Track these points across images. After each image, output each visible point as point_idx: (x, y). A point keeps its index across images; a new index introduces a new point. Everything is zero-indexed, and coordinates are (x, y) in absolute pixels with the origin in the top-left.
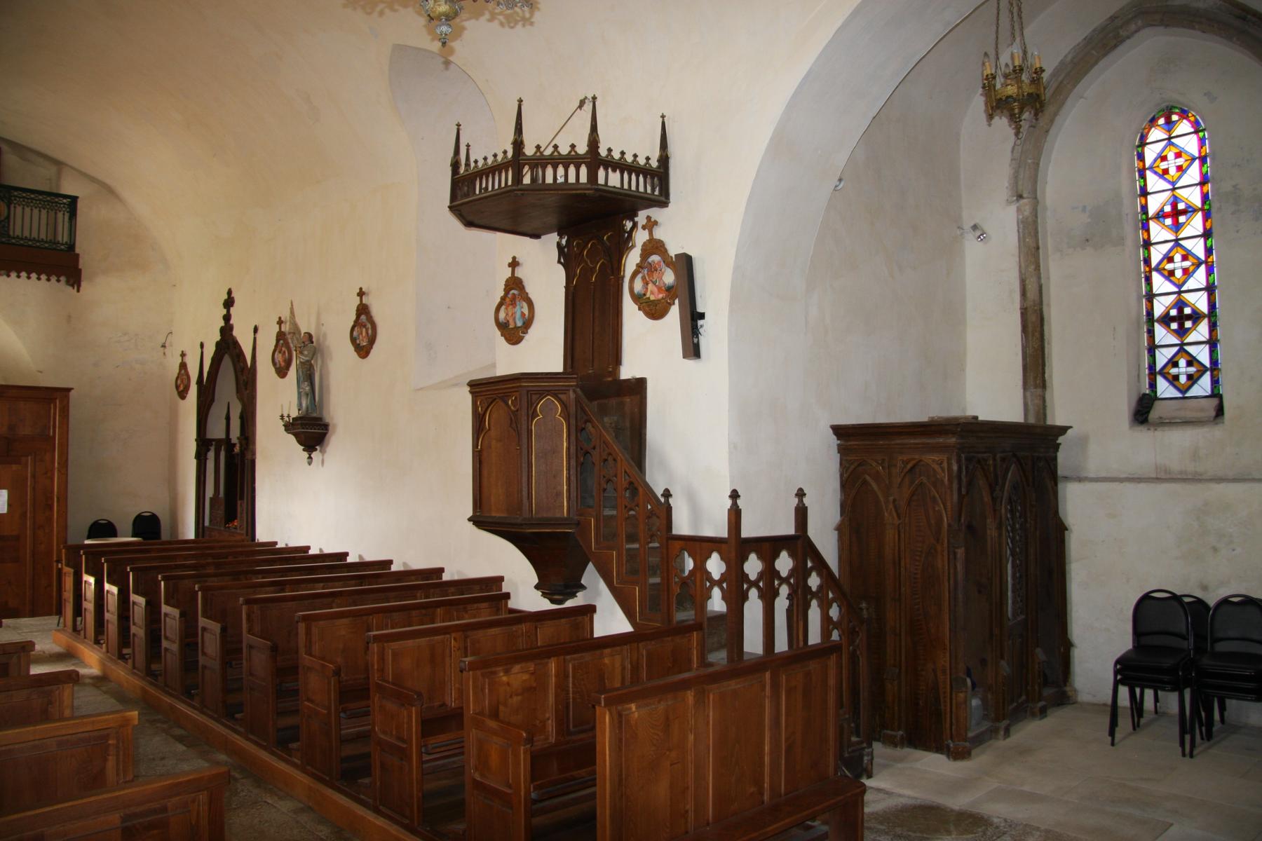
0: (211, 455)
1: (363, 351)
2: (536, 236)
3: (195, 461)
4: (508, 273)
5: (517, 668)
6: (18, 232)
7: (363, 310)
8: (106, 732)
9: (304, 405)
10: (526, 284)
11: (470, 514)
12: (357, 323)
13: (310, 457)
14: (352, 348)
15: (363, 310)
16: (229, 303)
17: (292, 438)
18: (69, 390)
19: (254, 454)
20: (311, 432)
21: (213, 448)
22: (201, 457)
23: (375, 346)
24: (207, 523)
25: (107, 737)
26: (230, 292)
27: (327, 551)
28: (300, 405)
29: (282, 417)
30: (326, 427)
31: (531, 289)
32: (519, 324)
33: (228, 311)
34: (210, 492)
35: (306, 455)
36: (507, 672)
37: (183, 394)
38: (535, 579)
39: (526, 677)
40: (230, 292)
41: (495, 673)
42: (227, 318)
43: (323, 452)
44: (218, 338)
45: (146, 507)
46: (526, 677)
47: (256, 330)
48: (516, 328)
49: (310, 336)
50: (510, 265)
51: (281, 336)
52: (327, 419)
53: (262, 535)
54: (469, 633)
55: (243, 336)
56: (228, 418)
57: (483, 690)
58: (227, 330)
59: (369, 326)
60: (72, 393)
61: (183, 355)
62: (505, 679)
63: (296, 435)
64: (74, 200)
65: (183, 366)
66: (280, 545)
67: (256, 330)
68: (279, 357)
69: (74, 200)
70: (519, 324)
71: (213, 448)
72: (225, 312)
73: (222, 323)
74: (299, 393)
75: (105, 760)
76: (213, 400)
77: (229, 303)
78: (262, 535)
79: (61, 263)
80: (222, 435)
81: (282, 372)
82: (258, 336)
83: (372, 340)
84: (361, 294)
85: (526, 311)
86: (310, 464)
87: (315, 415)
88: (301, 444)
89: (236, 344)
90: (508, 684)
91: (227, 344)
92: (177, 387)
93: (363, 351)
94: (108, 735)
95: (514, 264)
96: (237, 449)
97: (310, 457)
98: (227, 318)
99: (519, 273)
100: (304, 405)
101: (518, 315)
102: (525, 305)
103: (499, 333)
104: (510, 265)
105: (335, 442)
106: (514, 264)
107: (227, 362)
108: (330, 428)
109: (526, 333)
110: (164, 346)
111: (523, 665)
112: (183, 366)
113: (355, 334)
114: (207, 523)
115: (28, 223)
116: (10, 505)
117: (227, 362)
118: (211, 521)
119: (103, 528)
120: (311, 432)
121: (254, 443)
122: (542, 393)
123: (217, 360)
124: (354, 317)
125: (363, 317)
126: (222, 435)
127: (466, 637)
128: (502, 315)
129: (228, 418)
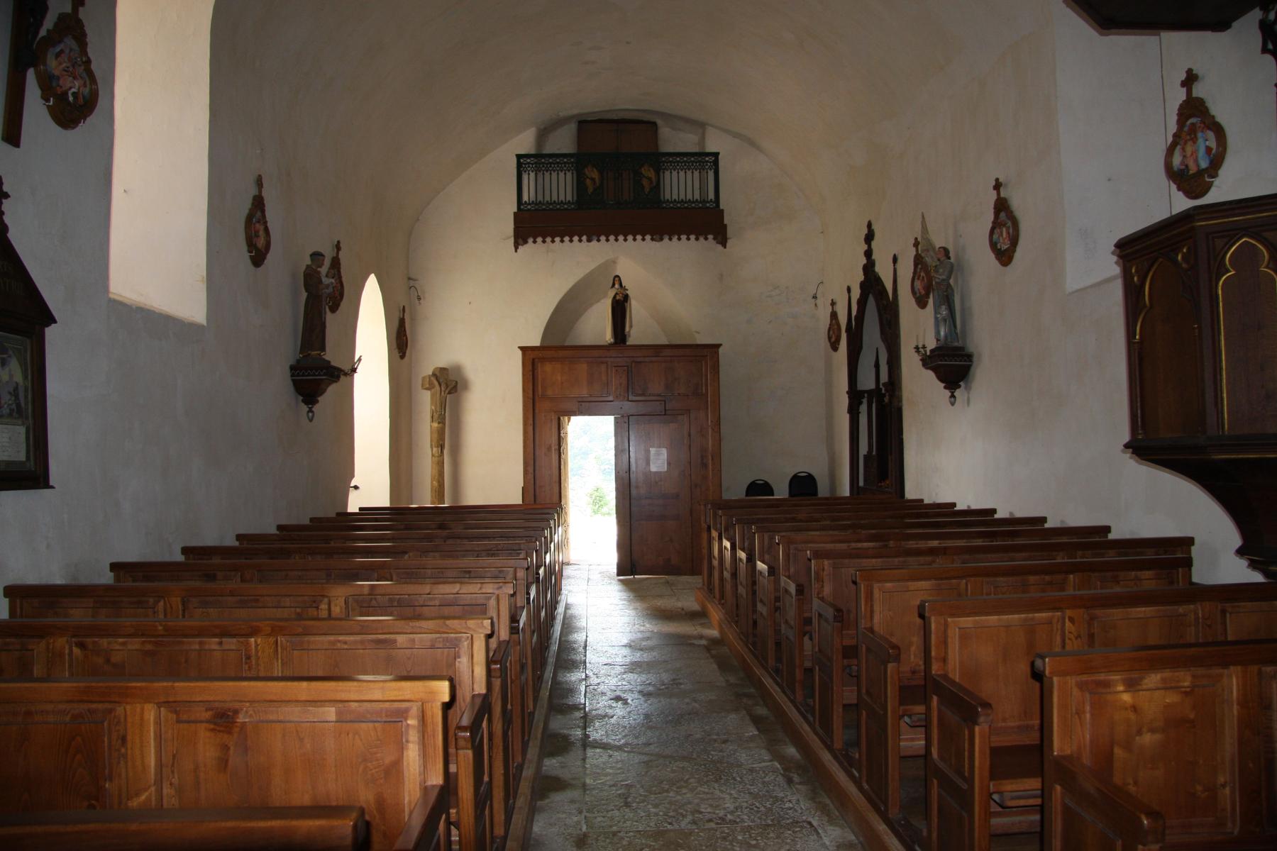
0: (864, 408)
1: (1005, 256)
2: (1221, 25)
3: (848, 416)
4: (1181, 95)
5: (1153, 679)
6: (668, 197)
7: (1002, 206)
8: (404, 705)
9: (942, 333)
10: (1210, 104)
11: (1126, 437)
12: (996, 225)
13: (953, 396)
14: (993, 256)
15: (1002, 206)
16: (869, 238)
17: (931, 375)
18: (719, 346)
19: (900, 400)
20: (953, 366)
21: (865, 401)
22: (853, 411)
23: (1019, 249)
24: (861, 484)
25: (404, 714)
26: (869, 225)
27: (973, 507)
28: (938, 333)
29: (917, 348)
30: (969, 357)
31: (1219, 111)
32: (1204, 164)
33: (870, 246)
34: (863, 449)
35: (948, 393)
36: (1131, 685)
37: (835, 347)
38: (1236, 541)
39: (1172, 698)
40: (869, 225)
41: (1107, 684)
42: (868, 254)
43: (968, 388)
44: (862, 278)
45: (803, 467)
46: (1172, 698)
47: (895, 260)
48: (1201, 173)
49: (946, 251)
50: (1183, 84)
51: (918, 260)
52: (971, 348)
53: (910, 493)
54: (1098, 612)
55: (884, 270)
56: (877, 366)
57: (1079, 713)
58: (869, 268)
59: (1009, 224)
60: (721, 350)
61: (833, 304)
62: (1126, 698)
63: (935, 369)
64: (716, 155)
65: (834, 315)
66: (926, 502)
67: (895, 260)
68: (918, 284)
69: (716, 155)
70: (1204, 164)
71: (865, 401)
72: (866, 247)
73: (864, 261)
74: (936, 318)
75: (401, 748)
76: (861, 348)
77: (869, 238)
78: (910, 493)
79: (707, 221)
80: (873, 386)
81: (922, 303)
82: (898, 266)
83: (1014, 241)
84: (998, 186)
85: (1212, 143)
86: (953, 404)
87: (956, 344)
88: (941, 381)
89: (878, 280)
90: (1134, 708)
91: (871, 283)
92: (830, 338)
93: (1005, 256)
94: (407, 711)
95: (1190, 79)
96: (886, 400)
97: (953, 396)
98: (868, 254)
99: (1199, 91)
100: (942, 333)
101: (1202, 151)
102: (1211, 135)
103: (1174, 187)
104: (1183, 84)
105: (982, 375)
106: (1190, 79)
107: (871, 303)
108: (975, 359)
109: (1215, 176)
110: (815, 297)
111: (1167, 674)
112: (834, 315)
113: (995, 237)
114: (861, 484)
115: (680, 186)
116: (669, 464)
117: (871, 303)
118: (865, 480)
119: (759, 488)
120: (953, 366)
121: (900, 388)
122: (1231, 234)
123: (862, 303)
124: (991, 217)
125: (1003, 215)
126: (873, 386)
127: (1092, 618)
128: (1177, 160)
129: (877, 366)
